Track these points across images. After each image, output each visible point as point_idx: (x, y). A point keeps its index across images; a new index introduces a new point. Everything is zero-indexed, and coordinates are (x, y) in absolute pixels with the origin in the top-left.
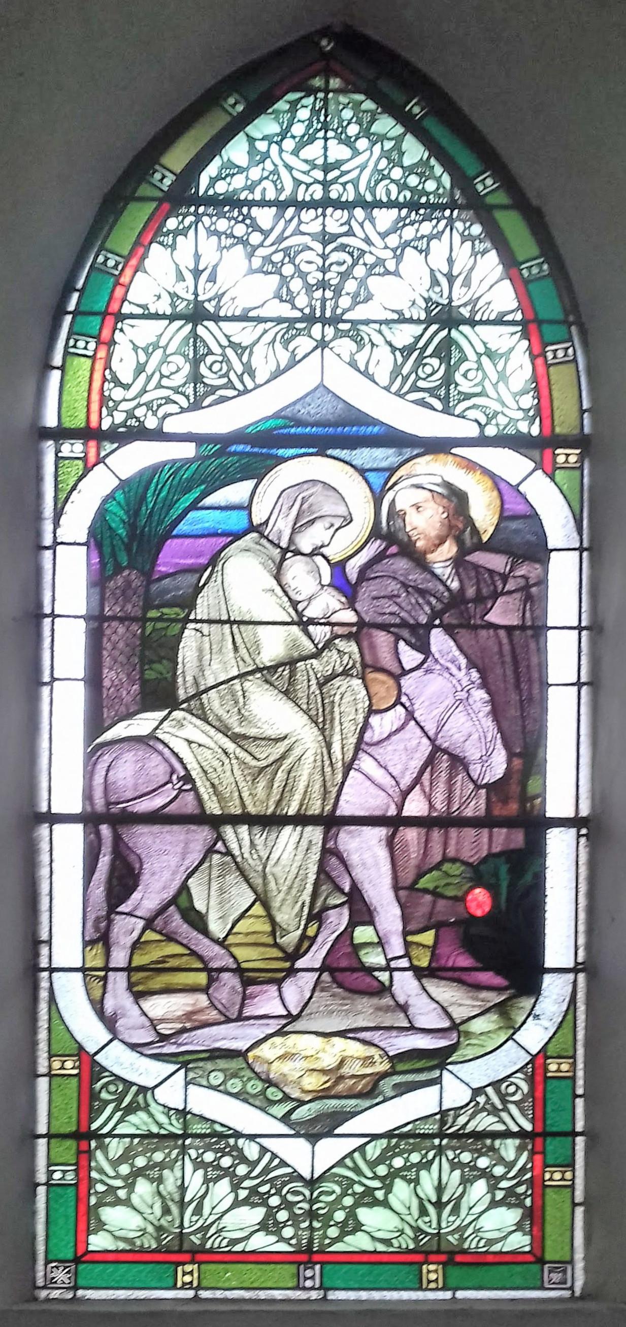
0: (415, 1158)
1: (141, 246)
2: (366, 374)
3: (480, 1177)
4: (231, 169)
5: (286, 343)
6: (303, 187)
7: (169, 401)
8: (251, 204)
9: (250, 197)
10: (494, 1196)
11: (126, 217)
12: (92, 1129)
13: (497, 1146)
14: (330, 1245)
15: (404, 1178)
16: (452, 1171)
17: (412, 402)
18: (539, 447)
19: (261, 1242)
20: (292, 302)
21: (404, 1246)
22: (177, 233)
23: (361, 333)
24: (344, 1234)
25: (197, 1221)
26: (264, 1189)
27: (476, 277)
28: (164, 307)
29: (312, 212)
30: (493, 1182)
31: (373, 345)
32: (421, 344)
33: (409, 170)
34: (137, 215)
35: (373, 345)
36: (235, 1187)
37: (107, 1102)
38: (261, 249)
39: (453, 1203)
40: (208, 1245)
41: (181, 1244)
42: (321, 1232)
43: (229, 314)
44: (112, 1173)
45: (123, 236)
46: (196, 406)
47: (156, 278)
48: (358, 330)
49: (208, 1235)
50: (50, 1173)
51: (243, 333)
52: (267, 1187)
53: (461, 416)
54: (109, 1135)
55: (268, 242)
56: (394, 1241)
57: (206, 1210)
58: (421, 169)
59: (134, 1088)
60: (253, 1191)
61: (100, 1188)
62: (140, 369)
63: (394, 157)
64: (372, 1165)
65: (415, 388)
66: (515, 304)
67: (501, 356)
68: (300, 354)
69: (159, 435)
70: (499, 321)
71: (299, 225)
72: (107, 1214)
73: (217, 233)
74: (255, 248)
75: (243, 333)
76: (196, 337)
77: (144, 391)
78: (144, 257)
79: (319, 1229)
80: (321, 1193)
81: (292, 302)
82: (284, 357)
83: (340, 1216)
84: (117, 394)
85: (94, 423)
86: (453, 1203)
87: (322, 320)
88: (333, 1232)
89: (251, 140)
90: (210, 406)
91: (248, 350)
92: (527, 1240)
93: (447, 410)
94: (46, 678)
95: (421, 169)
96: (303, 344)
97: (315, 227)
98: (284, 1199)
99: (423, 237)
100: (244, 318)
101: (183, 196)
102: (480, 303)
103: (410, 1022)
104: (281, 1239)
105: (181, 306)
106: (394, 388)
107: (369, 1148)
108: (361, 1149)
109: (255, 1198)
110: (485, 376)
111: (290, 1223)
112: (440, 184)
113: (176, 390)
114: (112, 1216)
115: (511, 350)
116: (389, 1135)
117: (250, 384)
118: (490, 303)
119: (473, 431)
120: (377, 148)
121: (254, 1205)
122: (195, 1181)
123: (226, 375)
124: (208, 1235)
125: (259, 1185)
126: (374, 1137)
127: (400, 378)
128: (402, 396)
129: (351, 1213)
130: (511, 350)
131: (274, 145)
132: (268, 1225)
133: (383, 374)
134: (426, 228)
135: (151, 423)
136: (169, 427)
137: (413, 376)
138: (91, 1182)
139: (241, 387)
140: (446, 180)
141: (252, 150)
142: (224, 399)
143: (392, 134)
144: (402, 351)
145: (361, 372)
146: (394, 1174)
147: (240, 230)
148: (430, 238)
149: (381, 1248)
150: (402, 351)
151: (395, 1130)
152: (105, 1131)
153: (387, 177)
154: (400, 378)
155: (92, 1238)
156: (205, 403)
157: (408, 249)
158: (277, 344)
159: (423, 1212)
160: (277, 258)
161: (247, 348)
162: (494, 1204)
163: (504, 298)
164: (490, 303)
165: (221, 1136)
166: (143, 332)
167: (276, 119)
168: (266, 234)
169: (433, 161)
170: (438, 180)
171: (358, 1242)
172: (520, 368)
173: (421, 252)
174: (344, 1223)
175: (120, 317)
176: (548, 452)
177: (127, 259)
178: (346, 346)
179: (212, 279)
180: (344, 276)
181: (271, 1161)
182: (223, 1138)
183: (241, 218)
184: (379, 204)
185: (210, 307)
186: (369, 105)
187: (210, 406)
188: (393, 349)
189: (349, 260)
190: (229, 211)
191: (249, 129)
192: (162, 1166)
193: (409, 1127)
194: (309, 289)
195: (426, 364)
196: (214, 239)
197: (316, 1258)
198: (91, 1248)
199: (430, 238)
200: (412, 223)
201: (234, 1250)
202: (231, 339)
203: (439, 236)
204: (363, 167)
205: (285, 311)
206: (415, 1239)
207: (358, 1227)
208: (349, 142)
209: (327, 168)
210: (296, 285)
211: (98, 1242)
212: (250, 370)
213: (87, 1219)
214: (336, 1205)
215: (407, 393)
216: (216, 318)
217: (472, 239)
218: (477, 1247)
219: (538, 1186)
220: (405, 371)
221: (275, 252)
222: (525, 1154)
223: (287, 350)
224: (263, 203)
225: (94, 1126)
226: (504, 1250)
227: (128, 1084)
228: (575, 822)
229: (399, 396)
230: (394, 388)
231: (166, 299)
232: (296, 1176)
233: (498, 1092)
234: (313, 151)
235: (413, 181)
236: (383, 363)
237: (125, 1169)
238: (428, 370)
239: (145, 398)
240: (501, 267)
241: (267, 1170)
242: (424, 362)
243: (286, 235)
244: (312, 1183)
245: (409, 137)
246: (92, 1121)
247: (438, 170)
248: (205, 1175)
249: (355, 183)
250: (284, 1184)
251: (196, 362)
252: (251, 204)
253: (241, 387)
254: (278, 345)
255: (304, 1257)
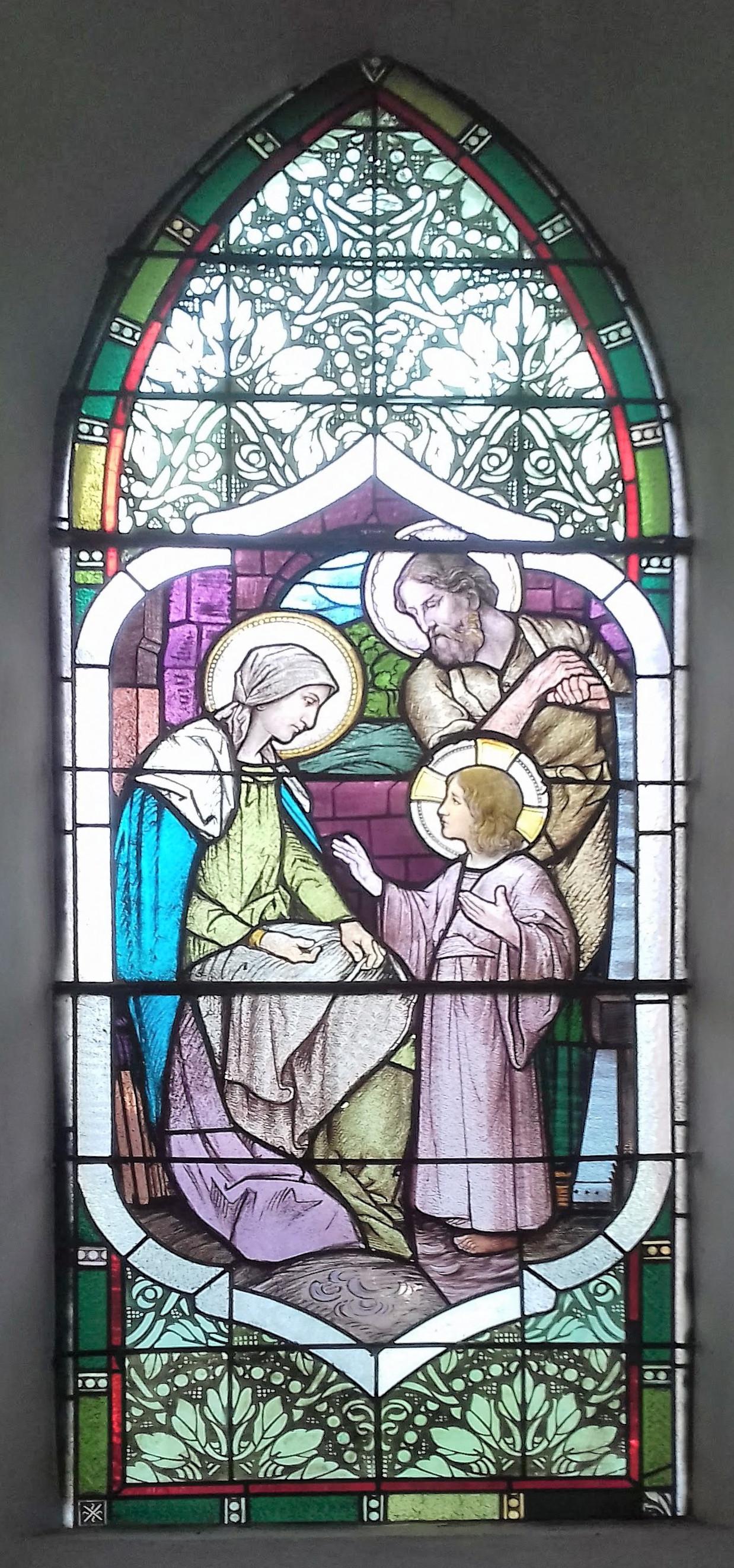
0: (496, 1370)
1: (160, 315)
2: (424, 465)
3: (566, 1392)
4: (264, 219)
5: (332, 431)
6: (349, 243)
7: (198, 499)
8: (289, 261)
9: (289, 253)
10: (584, 1412)
11: (142, 277)
12: (127, 1343)
13: (586, 1356)
14: (401, 1471)
15: (483, 1394)
16: (535, 1386)
17: (477, 498)
18: (633, 552)
19: (323, 1469)
20: (337, 380)
21: (485, 1471)
22: (202, 298)
23: (417, 415)
24: (415, 1459)
25: (246, 1447)
26: (323, 1407)
27: (550, 348)
28: (185, 385)
29: (359, 275)
30: (582, 1398)
31: (431, 430)
32: (486, 431)
33: (468, 224)
34: (155, 275)
35: (431, 430)
36: (288, 1407)
37: (146, 1311)
38: (301, 317)
39: (244, 1426)
40: (554, 1471)
41: (231, 1475)
42: (390, 1456)
43: (267, 392)
44: (149, 1395)
45: (141, 299)
46: (230, 505)
47: (183, 351)
48: (414, 412)
49: (554, 1459)
50: (671, 1375)
51: (283, 416)
52: (332, 1406)
53: (532, 515)
54: (152, 1350)
55: (309, 309)
56: (179, 1471)
57: (257, 1435)
58: (484, 224)
59: (174, 1296)
60: (309, 1410)
61: (137, 1412)
62: (165, 462)
63: (452, 207)
64: (447, 1378)
65: (479, 483)
66: (595, 381)
67: (576, 441)
68: (349, 440)
69: (190, 540)
70: (577, 401)
71: (344, 289)
72: (143, 1441)
73: (251, 297)
74: (294, 315)
75: (284, 416)
76: (228, 420)
77: (168, 487)
78: (166, 324)
79: (388, 1453)
80: (388, 1413)
81: (337, 380)
82: (331, 446)
83: (411, 1437)
84: (138, 489)
85: (110, 525)
86: (244, 1426)
87: (367, 403)
88: (404, 1456)
89: (292, 181)
90: (249, 502)
91: (289, 438)
92: (622, 1462)
93: (519, 509)
94: (69, 827)
95: (484, 224)
96: (351, 430)
97: (364, 292)
98: (344, 1418)
99: (488, 302)
100: (284, 396)
101: (195, 258)
102: (555, 378)
103: (232, 1235)
104: (343, 1465)
105: (210, 385)
106: (455, 481)
107: (444, 1360)
108: (434, 1361)
109: (312, 1419)
110: (559, 465)
111: (403, 1445)
112: (504, 239)
113: (205, 486)
114: (445, 1438)
115: (588, 434)
116: (464, 1345)
117: (292, 479)
118: (566, 378)
119: (545, 533)
120: (432, 198)
121: (309, 1427)
122: (537, 1396)
123: (554, 474)
124: (554, 1459)
125: (610, 1400)
126: (450, 1347)
127: (461, 471)
128: (466, 491)
129: (424, 1433)
130: (588, 434)
131: (317, 190)
132: (329, 1449)
133: (442, 465)
134: (491, 292)
135: (178, 527)
136: (200, 527)
137: (476, 469)
138: (125, 1405)
139: (282, 483)
140: (513, 235)
141: (294, 195)
142: (263, 496)
143: (450, 180)
144: (464, 438)
145: (415, 461)
146: (472, 1388)
147: (277, 293)
148: (496, 304)
149: (459, 1474)
150: (464, 438)
151: (473, 1337)
152: (145, 1345)
153: (442, 233)
154: (461, 471)
155: (131, 1471)
156: (243, 500)
157: (470, 317)
158: (323, 431)
159: (506, 1432)
160: (320, 327)
161: (288, 435)
162: (584, 1422)
163: (581, 373)
164: (566, 378)
165: (271, 1348)
166: (169, 415)
167: (323, 159)
168: (307, 298)
169: (497, 212)
170: (501, 235)
171: (434, 1467)
172: (598, 457)
173: (485, 320)
174: (417, 1445)
175: (139, 395)
176: (634, 558)
177: (145, 328)
178: (397, 431)
179: (246, 351)
180: (399, 348)
181: (328, 1375)
182: (274, 1351)
183: (278, 279)
184: (440, 263)
185: (244, 384)
186: (423, 145)
187: (249, 502)
188: (455, 435)
189: (404, 330)
190: (265, 271)
191: (290, 169)
192: (501, 1380)
193: (487, 1336)
194: (357, 366)
195: (490, 455)
196: (247, 304)
197: (239, 1489)
198: (129, 1481)
199: (496, 304)
200: (476, 285)
201: (290, 1478)
202: (270, 423)
203: (505, 302)
204: (415, 220)
205: (327, 388)
206: (498, 1465)
207: (433, 1449)
208: (399, 190)
209: (373, 221)
210: (342, 360)
211: (138, 1473)
212: (291, 461)
213: (121, 1450)
214: (407, 1425)
215: (470, 488)
216: (252, 398)
217: (546, 302)
218: (567, 1472)
219: (632, 1401)
220: (467, 463)
221: (317, 322)
222: (618, 1365)
223: (334, 437)
224: (307, 261)
225: (130, 1340)
226: (598, 1474)
227: (168, 1290)
228: (670, 988)
229: (462, 491)
230: (455, 481)
231: (192, 376)
232: (356, 1392)
233: (586, 1293)
234: (361, 203)
235: (473, 237)
236: (441, 451)
237: (163, 1390)
238: (494, 461)
239: (170, 497)
240: (579, 336)
241: (324, 1386)
242: (490, 451)
243: (329, 300)
244: (377, 1401)
245: (470, 183)
246: (125, 1333)
247: (503, 222)
248: (254, 1393)
249: (406, 239)
250: (346, 1401)
251: (520, 456)
252: (289, 261)
253: (282, 483)
254: (323, 431)
255: (372, 1487)
